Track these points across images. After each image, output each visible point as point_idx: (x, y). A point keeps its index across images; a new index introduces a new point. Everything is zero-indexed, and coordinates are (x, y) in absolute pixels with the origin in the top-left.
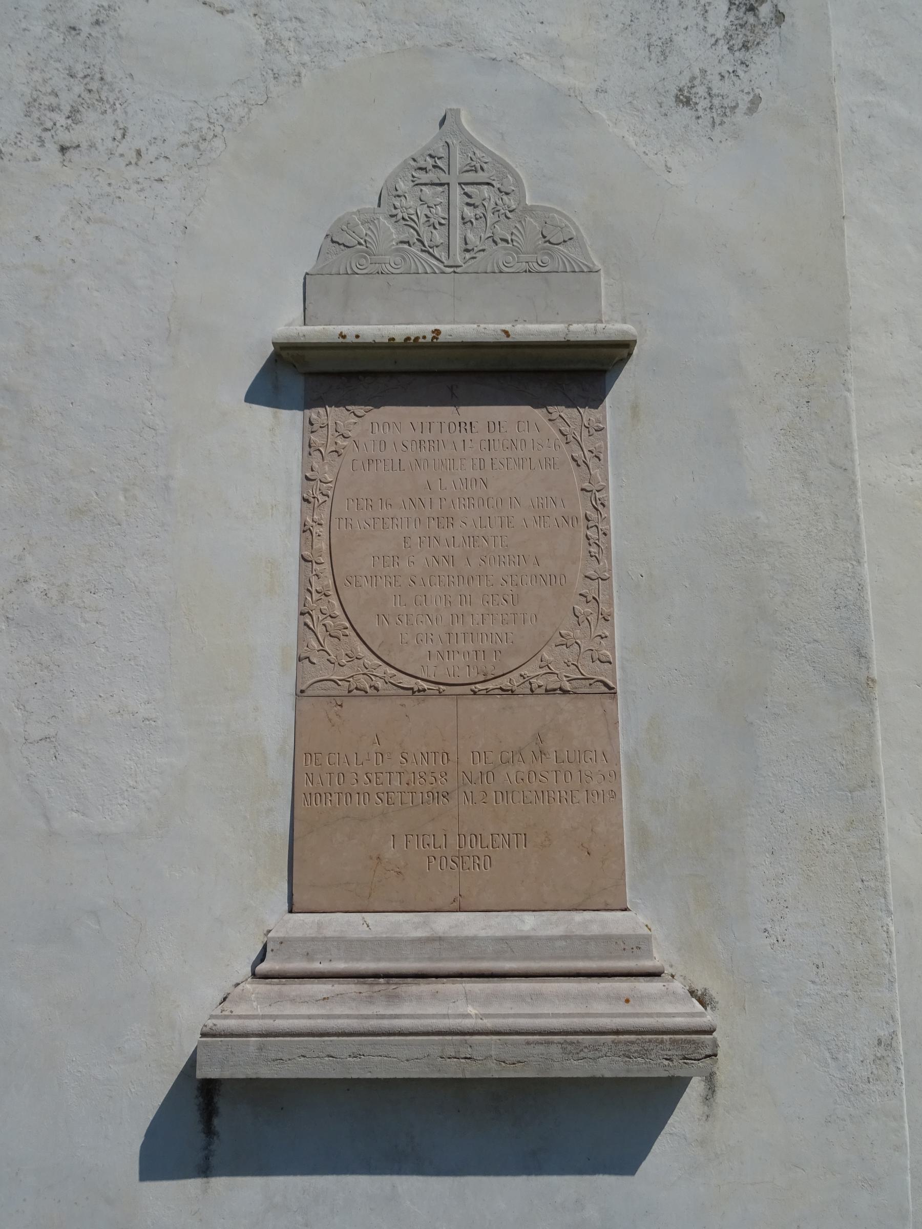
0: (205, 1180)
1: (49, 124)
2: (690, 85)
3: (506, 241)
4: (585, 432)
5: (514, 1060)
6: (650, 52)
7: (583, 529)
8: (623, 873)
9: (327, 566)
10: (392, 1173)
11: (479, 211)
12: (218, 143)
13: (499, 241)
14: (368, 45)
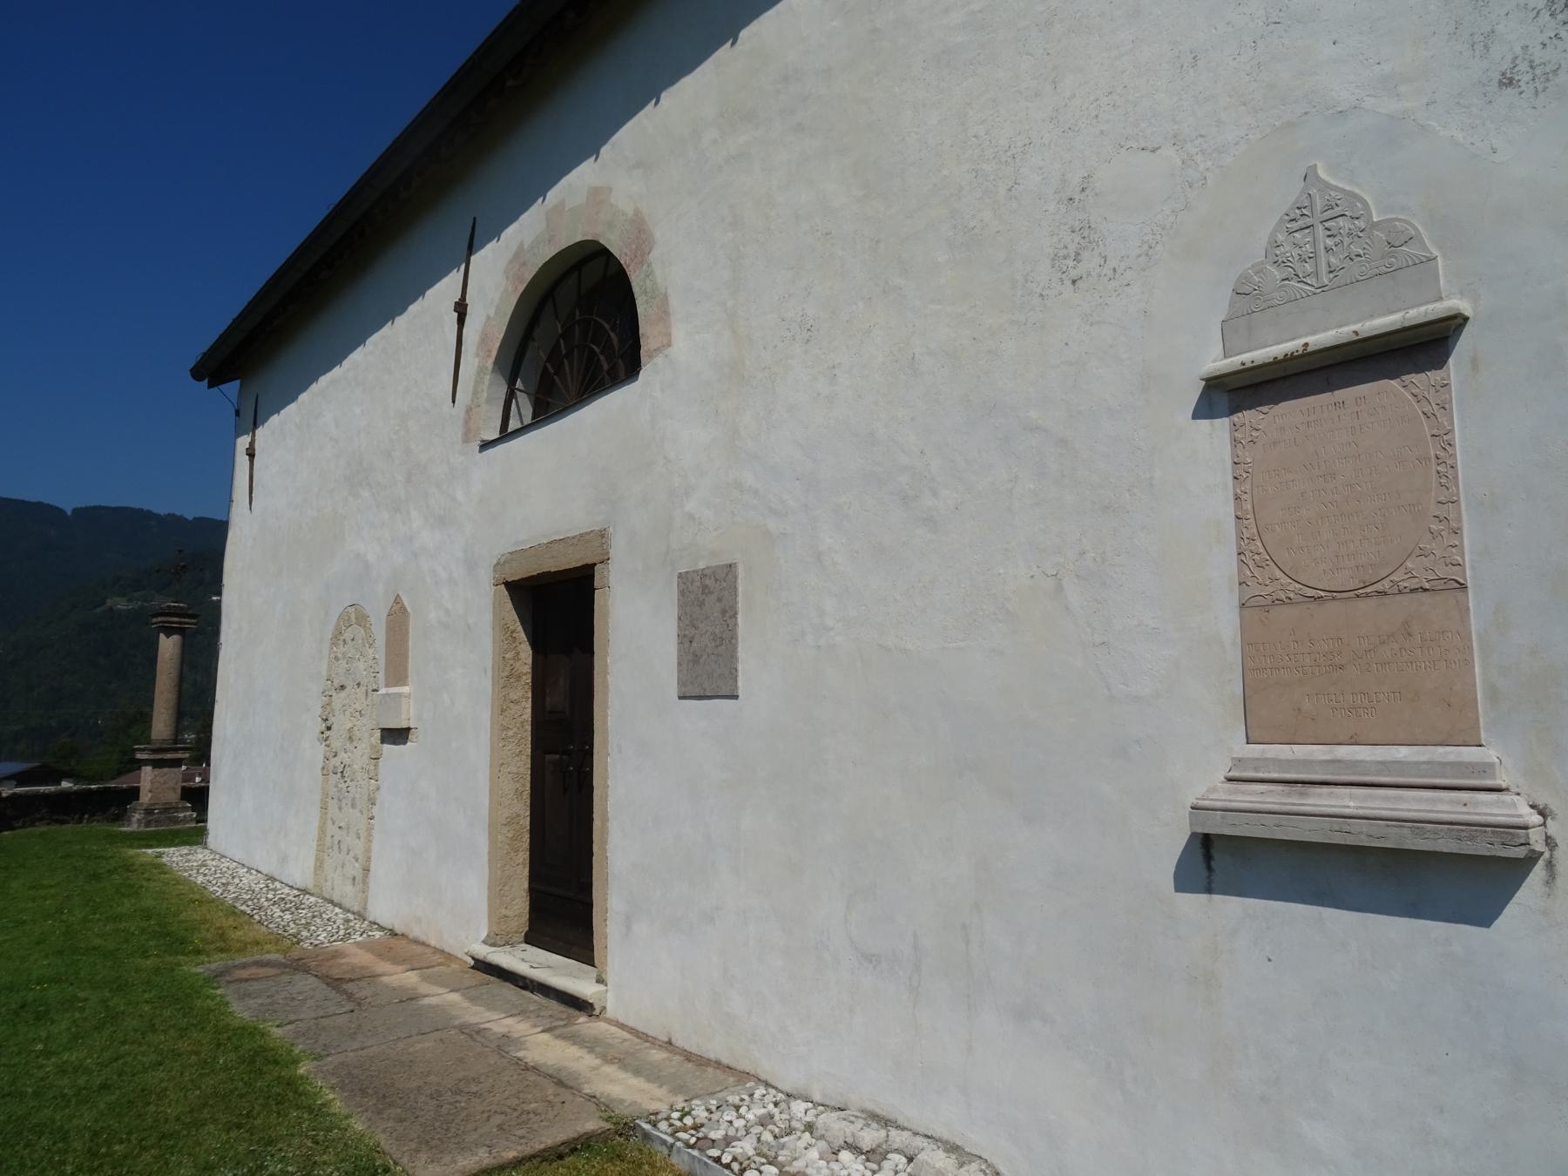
0: (1209, 895)
1: (1065, 268)
2: (1511, 66)
3: (1359, 256)
4: (1432, 390)
5: (1379, 835)
6: (1473, 50)
7: (1434, 467)
8: (1478, 719)
9: (1252, 520)
10: (1318, 905)
11: (1337, 240)
12: (1159, 247)
13: (1354, 257)
14: (1251, 136)
